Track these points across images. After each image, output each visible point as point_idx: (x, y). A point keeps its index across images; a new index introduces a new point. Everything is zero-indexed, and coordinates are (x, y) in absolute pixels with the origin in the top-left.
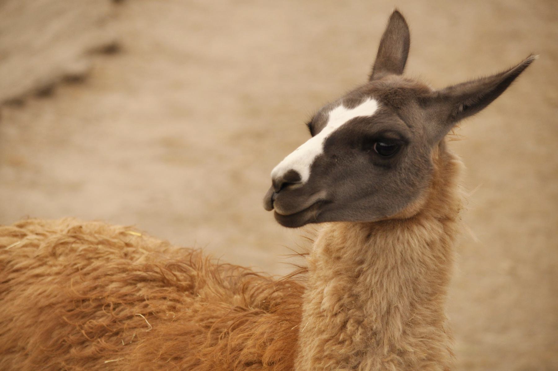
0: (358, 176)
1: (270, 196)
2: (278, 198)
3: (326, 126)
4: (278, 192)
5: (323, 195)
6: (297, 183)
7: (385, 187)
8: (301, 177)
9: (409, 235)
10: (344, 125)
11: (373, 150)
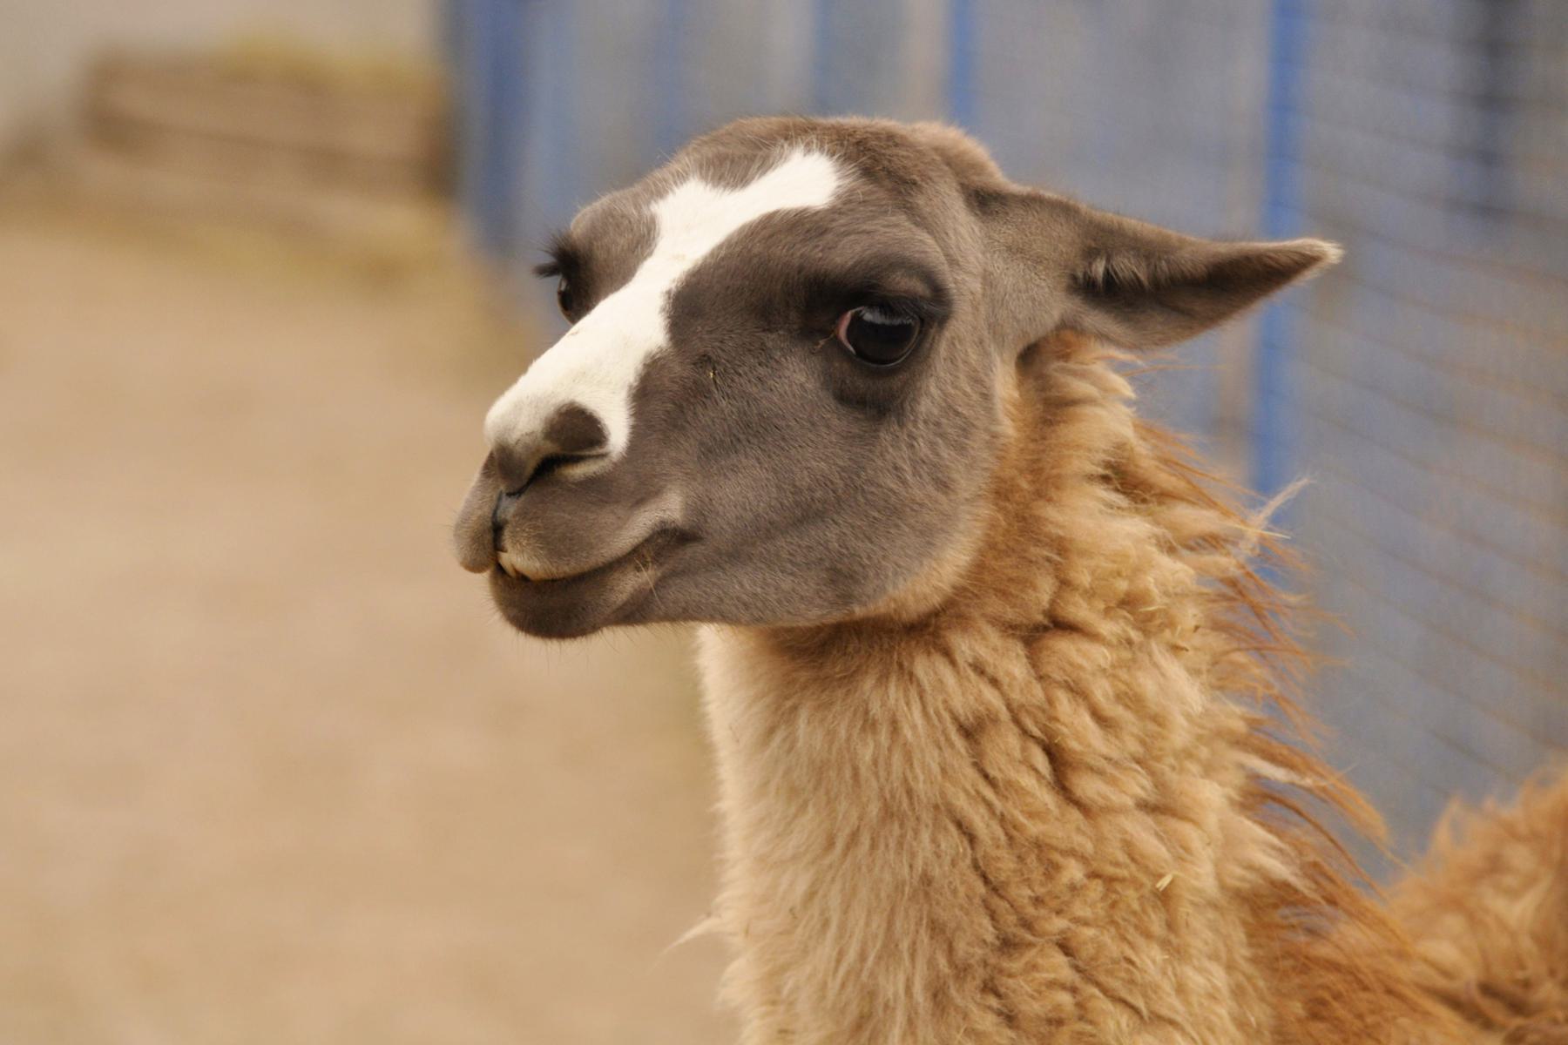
0: (784, 439)
1: (487, 510)
2: (522, 514)
3: (650, 254)
4: (514, 494)
5: (671, 507)
6: (590, 457)
7: (865, 487)
8: (606, 433)
9: (901, 694)
10: (729, 244)
11: (836, 342)
